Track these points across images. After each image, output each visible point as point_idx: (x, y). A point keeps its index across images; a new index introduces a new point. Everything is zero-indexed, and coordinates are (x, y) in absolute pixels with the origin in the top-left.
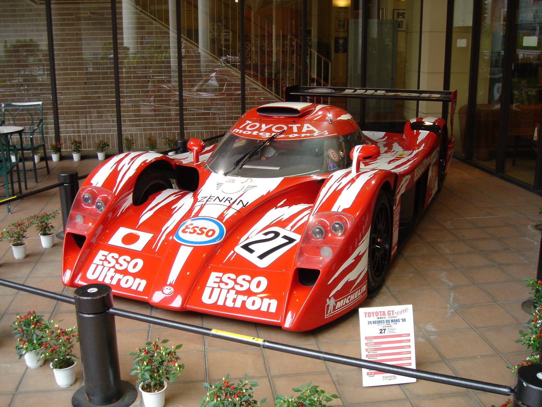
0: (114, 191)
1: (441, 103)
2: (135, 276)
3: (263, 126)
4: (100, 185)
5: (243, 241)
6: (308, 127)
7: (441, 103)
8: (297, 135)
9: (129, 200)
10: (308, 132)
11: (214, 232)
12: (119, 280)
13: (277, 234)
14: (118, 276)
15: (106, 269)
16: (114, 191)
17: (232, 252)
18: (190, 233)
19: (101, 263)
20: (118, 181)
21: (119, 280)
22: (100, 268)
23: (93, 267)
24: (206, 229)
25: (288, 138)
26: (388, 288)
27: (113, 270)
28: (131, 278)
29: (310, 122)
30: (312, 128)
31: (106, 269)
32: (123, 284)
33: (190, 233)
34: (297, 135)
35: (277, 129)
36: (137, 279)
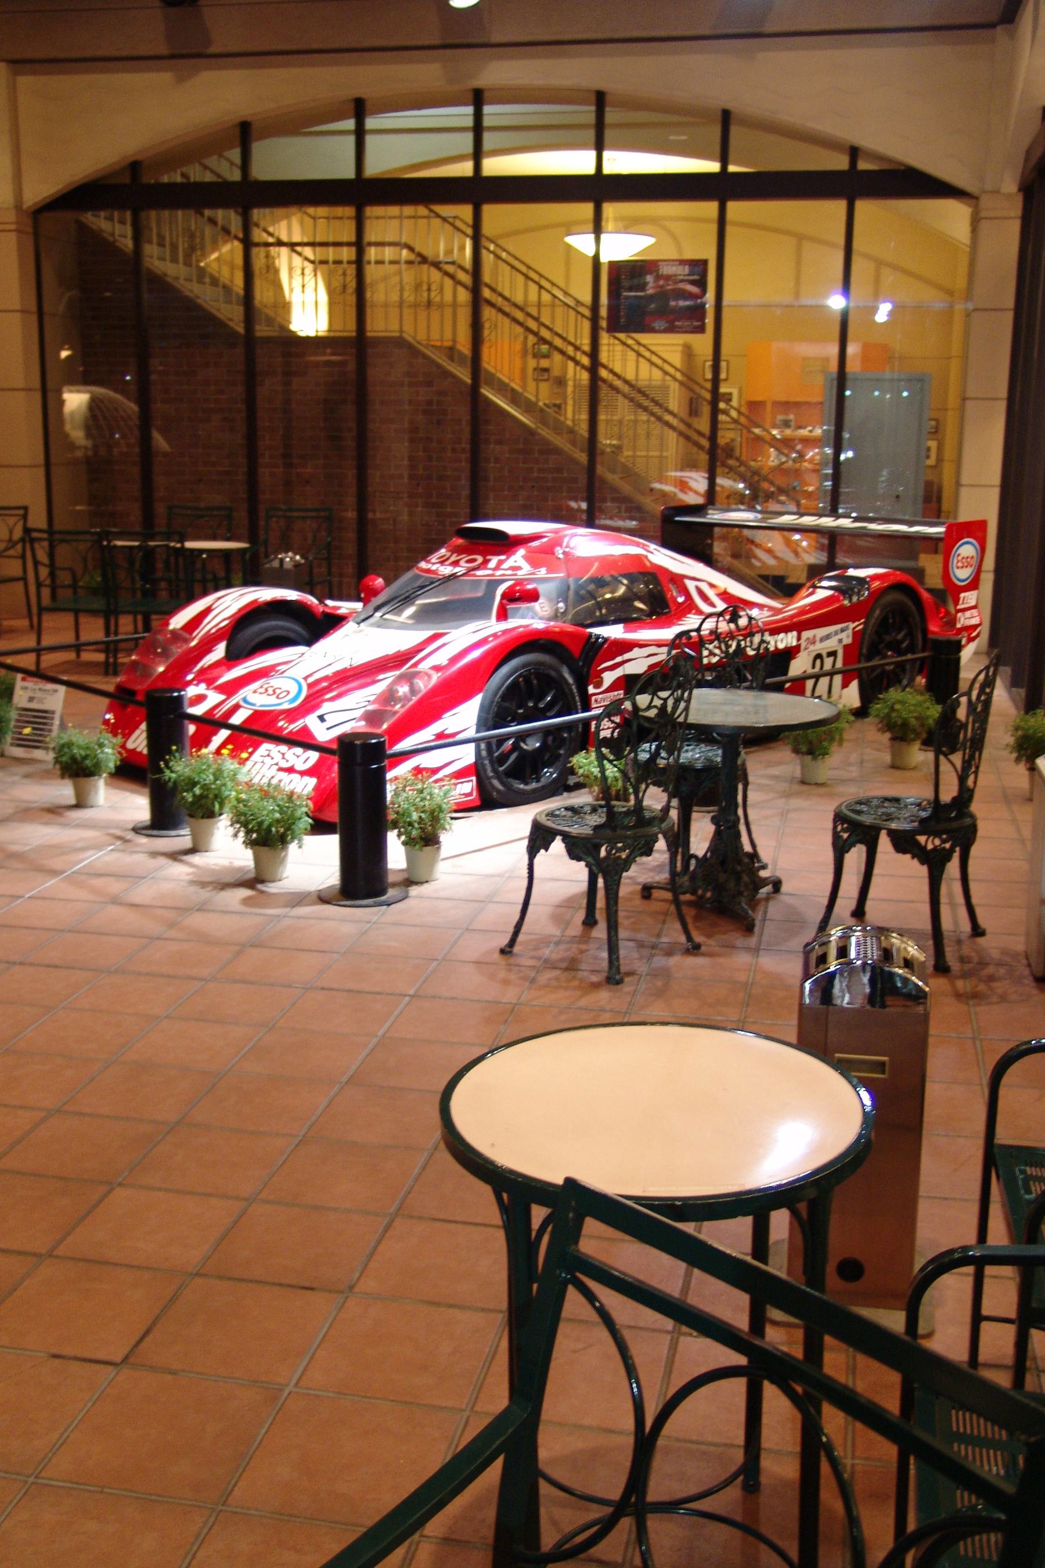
9: (219, 652)
11: (288, 692)
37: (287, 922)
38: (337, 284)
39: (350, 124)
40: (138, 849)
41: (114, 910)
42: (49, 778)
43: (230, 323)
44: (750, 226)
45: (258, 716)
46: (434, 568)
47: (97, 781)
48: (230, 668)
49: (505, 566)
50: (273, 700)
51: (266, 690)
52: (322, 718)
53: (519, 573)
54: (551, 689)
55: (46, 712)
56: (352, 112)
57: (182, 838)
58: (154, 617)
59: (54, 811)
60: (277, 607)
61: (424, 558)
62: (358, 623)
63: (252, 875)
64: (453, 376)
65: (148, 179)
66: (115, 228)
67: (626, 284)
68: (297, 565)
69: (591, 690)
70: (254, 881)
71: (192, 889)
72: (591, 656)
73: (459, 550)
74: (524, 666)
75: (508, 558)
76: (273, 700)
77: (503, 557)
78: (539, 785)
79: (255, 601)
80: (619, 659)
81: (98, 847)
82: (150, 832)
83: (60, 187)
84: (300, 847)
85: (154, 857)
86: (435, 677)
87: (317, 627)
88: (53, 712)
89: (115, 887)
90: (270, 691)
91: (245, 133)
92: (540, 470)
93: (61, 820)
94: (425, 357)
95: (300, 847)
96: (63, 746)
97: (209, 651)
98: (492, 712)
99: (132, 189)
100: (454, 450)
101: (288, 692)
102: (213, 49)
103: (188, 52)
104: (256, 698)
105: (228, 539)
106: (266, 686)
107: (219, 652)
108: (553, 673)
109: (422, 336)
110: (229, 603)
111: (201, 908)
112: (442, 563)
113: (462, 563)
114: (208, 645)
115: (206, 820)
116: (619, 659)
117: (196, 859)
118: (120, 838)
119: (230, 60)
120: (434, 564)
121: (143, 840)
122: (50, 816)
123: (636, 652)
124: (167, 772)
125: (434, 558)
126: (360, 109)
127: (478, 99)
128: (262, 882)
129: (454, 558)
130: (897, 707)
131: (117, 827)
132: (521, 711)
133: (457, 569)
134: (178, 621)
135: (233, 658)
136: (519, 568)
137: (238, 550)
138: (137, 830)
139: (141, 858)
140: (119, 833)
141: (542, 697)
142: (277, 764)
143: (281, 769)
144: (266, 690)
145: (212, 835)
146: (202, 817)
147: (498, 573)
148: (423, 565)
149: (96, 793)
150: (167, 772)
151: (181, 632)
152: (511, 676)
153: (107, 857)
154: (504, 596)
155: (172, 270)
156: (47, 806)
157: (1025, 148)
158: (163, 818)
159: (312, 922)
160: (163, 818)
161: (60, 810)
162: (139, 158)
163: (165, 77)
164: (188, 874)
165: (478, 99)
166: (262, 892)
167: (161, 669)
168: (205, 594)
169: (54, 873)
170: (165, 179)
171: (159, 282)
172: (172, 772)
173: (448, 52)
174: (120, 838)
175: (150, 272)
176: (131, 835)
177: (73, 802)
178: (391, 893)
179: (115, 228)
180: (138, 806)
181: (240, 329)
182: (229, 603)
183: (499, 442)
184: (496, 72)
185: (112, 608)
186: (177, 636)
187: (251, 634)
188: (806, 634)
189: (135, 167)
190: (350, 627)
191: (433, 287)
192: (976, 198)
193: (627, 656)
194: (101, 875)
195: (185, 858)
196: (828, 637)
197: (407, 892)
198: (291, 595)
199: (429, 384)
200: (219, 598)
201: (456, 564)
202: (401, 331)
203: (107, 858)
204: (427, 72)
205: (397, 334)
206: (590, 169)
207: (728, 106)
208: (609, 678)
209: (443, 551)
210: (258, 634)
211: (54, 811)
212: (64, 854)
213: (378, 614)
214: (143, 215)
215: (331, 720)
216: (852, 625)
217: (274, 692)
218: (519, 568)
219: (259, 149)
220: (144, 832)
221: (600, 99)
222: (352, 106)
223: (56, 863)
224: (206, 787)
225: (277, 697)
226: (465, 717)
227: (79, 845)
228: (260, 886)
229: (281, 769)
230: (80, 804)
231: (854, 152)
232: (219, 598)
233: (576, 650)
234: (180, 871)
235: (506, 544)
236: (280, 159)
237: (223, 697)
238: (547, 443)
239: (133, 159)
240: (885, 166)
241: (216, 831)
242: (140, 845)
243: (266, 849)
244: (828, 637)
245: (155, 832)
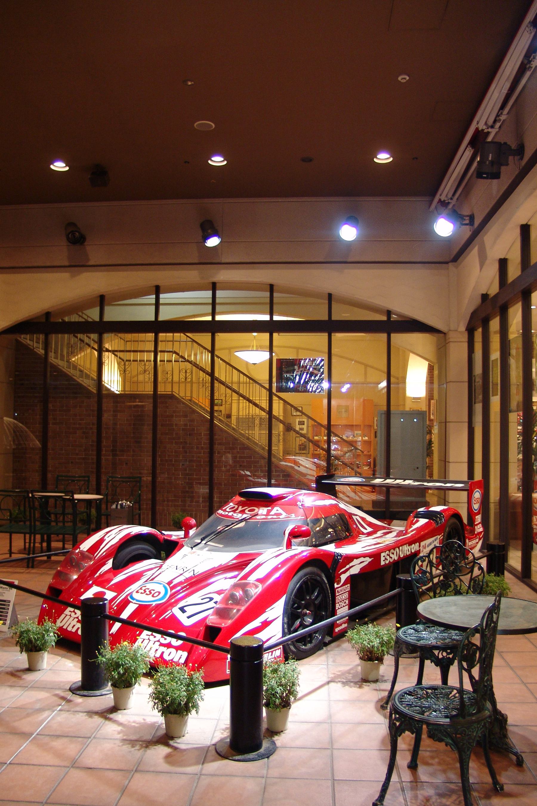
0: (95, 555)
1: (466, 493)
2: (177, 648)
3: (240, 507)
4: (85, 550)
5: (181, 604)
6: (277, 510)
7: (466, 493)
8: (264, 517)
9: (109, 564)
10: (276, 514)
11: (159, 593)
12: (163, 653)
13: (211, 599)
14: (163, 649)
15: (72, 618)
16: (95, 555)
17: (170, 611)
18: (141, 593)
19: (70, 613)
20: (101, 547)
21: (163, 653)
22: (68, 617)
23: (63, 616)
24: (154, 590)
25: (279, 518)
26: (327, 657)
27: (77, 620)
28: (173, 650)
29: (282, 506)
30: (280, 511)
31: (72, 618)
32: (166, 657)
33: (141, 593)
34: (264, 517)
35: (249, 511)
36: (179, 651)
37: (205, 781)
38: (142, 369)
39: (152, 299)
40: (78, 709)
41: (76, 775)
42: (8, 646)
43: (89, 388)
44: (308, 349)
45: (142, 609)
46: (230, 514)
47: (43, 654)
48: (115, 575)
49: (272, 513)
50: (149, 598)
51: (145, 591)
52: (182, 610)
53: (281, 517)
54: (316, 588)
55: (5, 601)
56: (154, 292)
57: (106, 696)
58: (52, 536)
59: (15, 674)
60: (139, 537)
61: (220, 507)
62: (192, 548)
63: (162, 732)
64: (198, 413)
65: (52, 320)
66: (35, 343)
67: (284, 370)
68: (129, 506)
69: (336, 586)
70: (166, 738)
71: (126, 748)
72: (330, 566)
73: (243, 504)
74: (305, 575)
75: (272, 509)
76: (149, 598)
77: (270, 508)
78: (312, 645)
79: (129, 534)
80: (348, 567)
81: (51, 708)
82: (82, 692)
83: (11, 323)
84: (197, 713)
85: (91, 717)
86: (260, 588)
87: (166, 549)
88: (9, 602)
89: (71, 749)
90: (148, 592)
91: (102, 301)
92: (240, 457)
93: (21, 682)
94: (184, 403)
95: (197, 713)
96: (22, 633)
97: (104, 564)
98: (290, 605)
99: (46, 325)
100: (197, 448)
101: (159, 593)
102: (91, 263)
103: (78, 265)
104: (139, 595)
105: (87, 493)
106: (144, 588)
107: (109, 564)
108: (318, 578)
109: (182, 394)
110: (114, 535)
111: (137, 768)
112: (234, 511)
113: (246, 511)
114: (102, 562)
115: (125, 689)
116: (348, 567)
117: (119, 716)
118: (63, 698)
119: (98, 268)
120: (229, 512)
121: (79, 700)
122: (13, 679)
123: (355, 562)
124: (100, 657)
125: (228, 508)
126: (158, 291)
127: (214, 287)
128: (172, 738)
129: (240, 509)
130: (490, 584)
131: (60, 689)
132: (303, 602)
133: (245, 516)
134: (86, 546)
135: (117, 568)
136: (281, 514)
137: (96, 500)
138: (73, 690)
139: (82, 717)
140: (62, 694)
141: (313, 593)
142: (159, 641)
143: (161, 645)
144: (145, 591)
145: (129, 698)
146: (124, 688)
147: (269, 517)
148: (220, 512)
149: (42, 661)
150: (100, 657)
151: (87, 553)
152: (299, 582)
153: (58, 718)
154: (290, 534)
155: (61, 364)
156: (9, 669)
157: (471, 312)
158: (90, 682)
159: (223, 779)
160: (90, 682)
161: (19, 674)
162: (50, 311)
163: (64, 275)
164: (119, 733)
165: (214, 287)
166: (176, 748)
167: (75, 577)
168: (98, 529)
169: (25, 735)
170: (66, 319)
171: (55, 368)
172: (103, 656)
173: (201, 266)
174: (63, 698)
175: (51, 363)
176: (69, 696)
177: (26, 666)
178: (265, 744)
179: (35, 343)
180: (67, 669)
181: (94, 391)
182: (114, 535)
183: (220, 444)
184: (223, 275)
185: (33, 531)
186: (83, 556)
187: (126, 554)
188: (422, 544)
189: (48, 314)
190: (185, 550)
191: (188, 371)
192: (445, 334)
193: (351, 564)
194: (58, 736)
195: (111, 716)
196: (430, 544)
197: (274, 743)
198: (145, 530)
199: (186, 416)
200: (107, 533)
201: (243, 512)
202: (172, 391)
203: (59, 719)
204: (191, 275)
205: (171, 393)
206: (269, 319)
207: (332, 292)
208: (343, 577)
209: (231, 504)
210: (130, 553)
211: (15, 674)
212: (28, 715)
213: (204, 542)
214: (50, 336)
215: (190, 610)
216: (439, 537)
217: (151, 593)
218: (281, 514)
219: (108, 310)
220: (78, 692)
221: (272, 288)
222: (154, 289)
223: (24, 725)
224: (126, 670)
225: (153, 596)
226: (277, 610)
227: (38, 706)
228: (171, 742)
229: (161, 645)
230: (30, 669)
231: (389, 313)
232: (107, 533)
233: (329, 564)
234: (110, 729)
235: (268, 501)
236: (114, 313)
237: (115, 594)
238: (243, 444)
239: (47, 311)
240: (407, 319)
241: (131, 695)
242: (77, 705)
243: (175, 715)
244: (430, 544)
245: (85, 693)
